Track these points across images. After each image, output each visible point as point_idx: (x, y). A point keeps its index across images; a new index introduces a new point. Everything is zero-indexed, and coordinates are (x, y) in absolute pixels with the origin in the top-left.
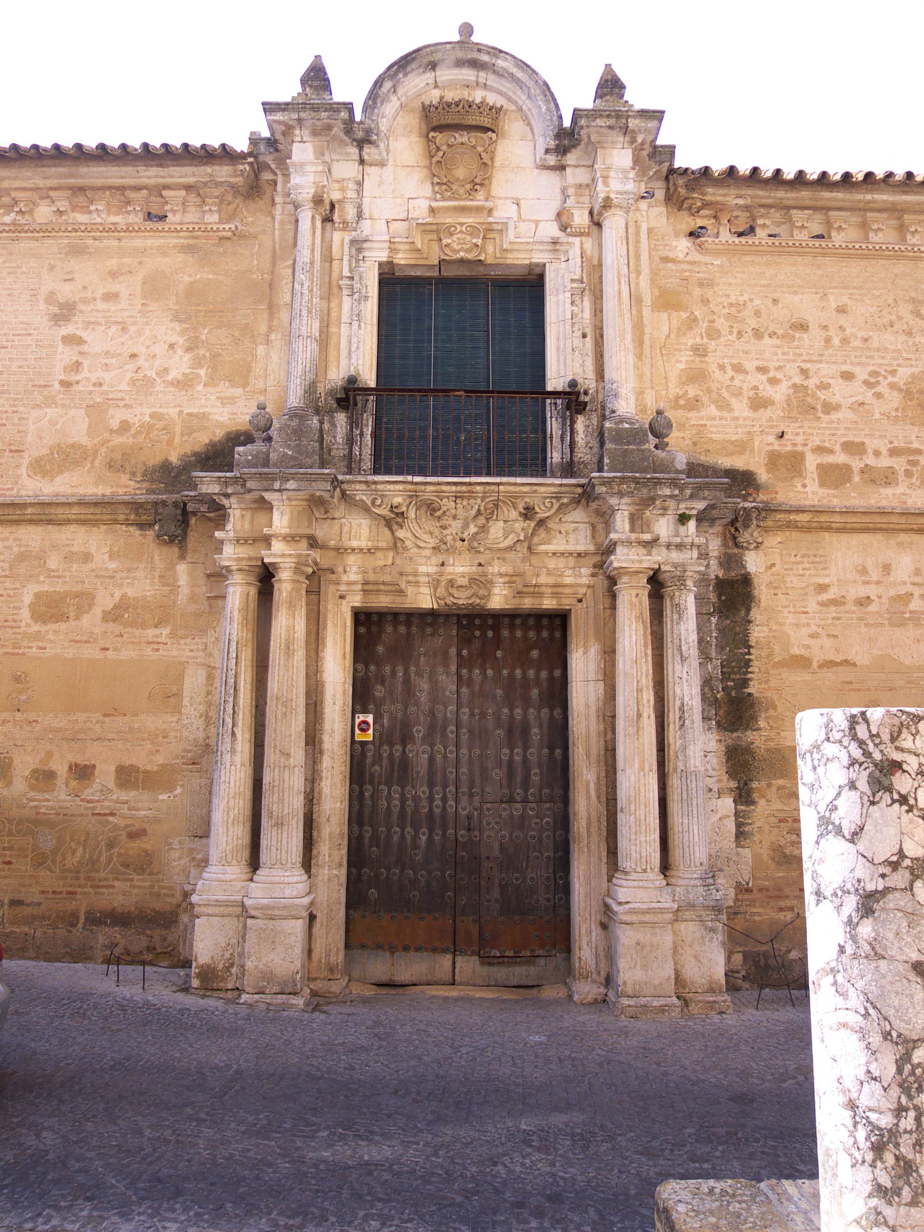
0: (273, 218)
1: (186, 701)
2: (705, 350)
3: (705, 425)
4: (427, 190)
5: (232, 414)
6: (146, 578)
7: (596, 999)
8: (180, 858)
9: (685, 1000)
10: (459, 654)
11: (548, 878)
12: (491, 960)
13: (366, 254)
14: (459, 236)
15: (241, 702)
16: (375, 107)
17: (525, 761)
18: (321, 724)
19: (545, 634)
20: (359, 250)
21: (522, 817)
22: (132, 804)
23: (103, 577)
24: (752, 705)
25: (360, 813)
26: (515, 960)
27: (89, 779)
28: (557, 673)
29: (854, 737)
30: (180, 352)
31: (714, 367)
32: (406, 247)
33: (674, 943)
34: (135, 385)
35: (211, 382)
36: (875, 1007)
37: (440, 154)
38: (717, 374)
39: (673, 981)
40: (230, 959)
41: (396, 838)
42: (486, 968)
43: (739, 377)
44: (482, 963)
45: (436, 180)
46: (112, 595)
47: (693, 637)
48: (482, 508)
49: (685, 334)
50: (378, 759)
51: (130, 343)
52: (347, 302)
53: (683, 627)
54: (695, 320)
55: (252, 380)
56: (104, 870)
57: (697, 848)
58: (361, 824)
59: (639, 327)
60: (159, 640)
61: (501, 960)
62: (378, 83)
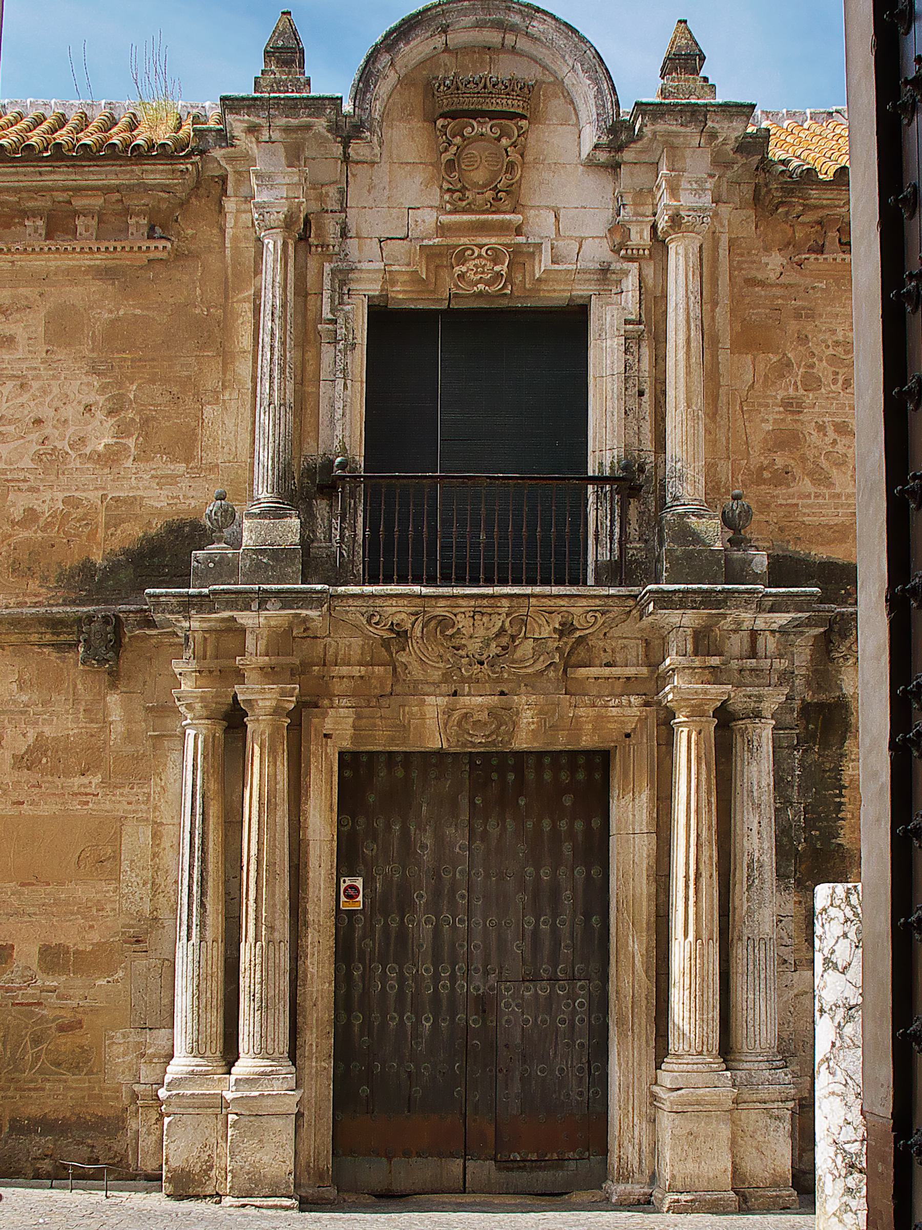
0: (223, 231)
1: (125, 866)
2: (799, 405)
3: (797, 505)
4: (434, 197)
5: (173, 498)
6: (67, 712)
7: (639, 1200)
8: (124, 1055)
9: (744, 1195)
10: (472, 803)
11: (581, 1070)
12: (510, 1165)
13: (353, 286)
14: (477, 261)
15: (211, 867)
16: (368, 91)
17: (554, 930)
18: (306, 891)
19: (581, 776)
20: (343, 283)
21: (549, 998)
22: (62, 990)
23: (12, 712)
24: (843, 858)
25: (348, 996)
26: (540, 1164)
27: (6, 963)
28: (596, 823)
29: (849, 904)
30: (100, 415)
31: (811, 428)
32: (406, 278)
33: (733, 1133)
34: (41, 460)
35: (143, 456)
36: (851, 1079)
37: (453, 149)
38: (815, 437)
39: (729, 1174)
40: (207, 1161)
41: (392, 1024)
42: (504, 1174)
43: (843, 441)
44: (499, 1169)
45: (446, 186)
46: (24, 735)
47: (768, 780)
48: (507, 624)
49: (774, 383)
50: (369, 932)
51: (32, 404)
52: (327, 352)
53: (754, 768)
54: (789, 364)
55: (198, 452)
56: (30, 1070)
57: (763, 1028)
58: (349, 1010)
59: (712, 376)
60: (88, 790)
61: (521, 1164)
62: (372, 58)
